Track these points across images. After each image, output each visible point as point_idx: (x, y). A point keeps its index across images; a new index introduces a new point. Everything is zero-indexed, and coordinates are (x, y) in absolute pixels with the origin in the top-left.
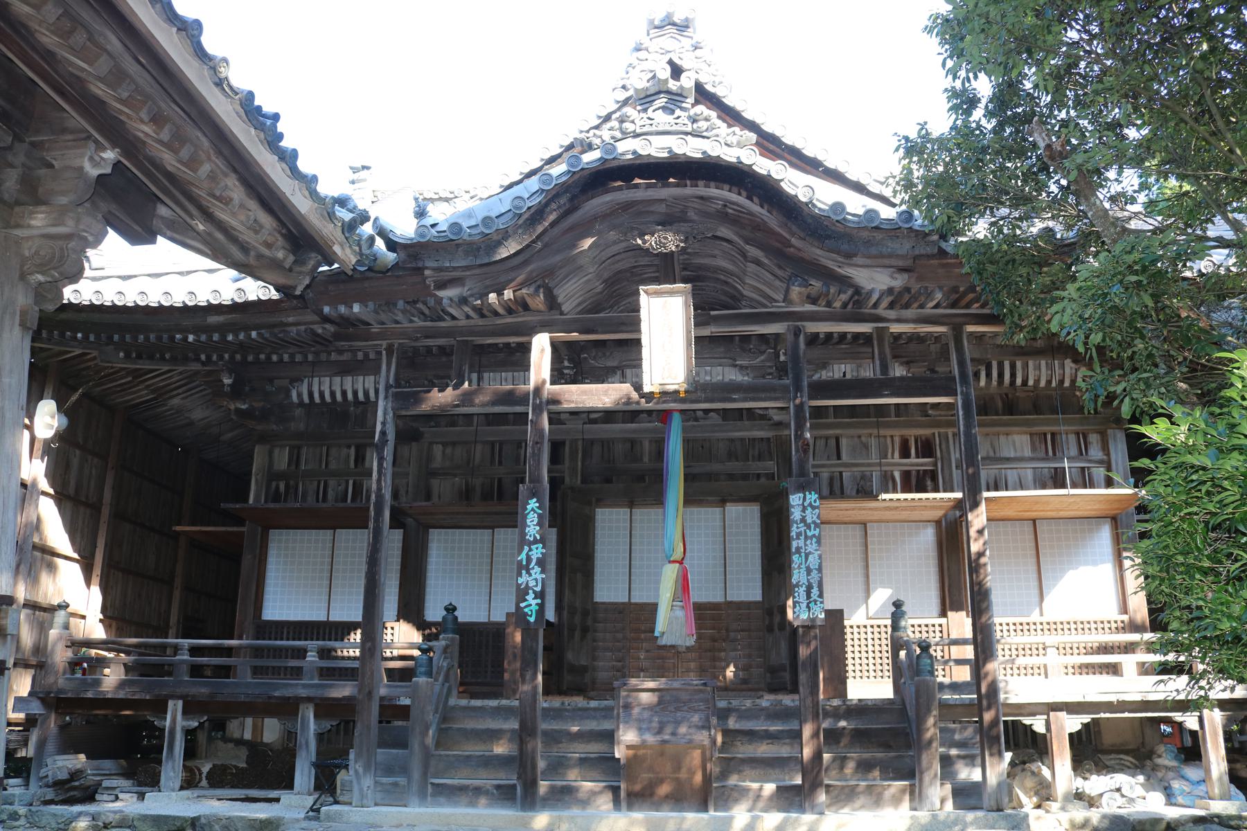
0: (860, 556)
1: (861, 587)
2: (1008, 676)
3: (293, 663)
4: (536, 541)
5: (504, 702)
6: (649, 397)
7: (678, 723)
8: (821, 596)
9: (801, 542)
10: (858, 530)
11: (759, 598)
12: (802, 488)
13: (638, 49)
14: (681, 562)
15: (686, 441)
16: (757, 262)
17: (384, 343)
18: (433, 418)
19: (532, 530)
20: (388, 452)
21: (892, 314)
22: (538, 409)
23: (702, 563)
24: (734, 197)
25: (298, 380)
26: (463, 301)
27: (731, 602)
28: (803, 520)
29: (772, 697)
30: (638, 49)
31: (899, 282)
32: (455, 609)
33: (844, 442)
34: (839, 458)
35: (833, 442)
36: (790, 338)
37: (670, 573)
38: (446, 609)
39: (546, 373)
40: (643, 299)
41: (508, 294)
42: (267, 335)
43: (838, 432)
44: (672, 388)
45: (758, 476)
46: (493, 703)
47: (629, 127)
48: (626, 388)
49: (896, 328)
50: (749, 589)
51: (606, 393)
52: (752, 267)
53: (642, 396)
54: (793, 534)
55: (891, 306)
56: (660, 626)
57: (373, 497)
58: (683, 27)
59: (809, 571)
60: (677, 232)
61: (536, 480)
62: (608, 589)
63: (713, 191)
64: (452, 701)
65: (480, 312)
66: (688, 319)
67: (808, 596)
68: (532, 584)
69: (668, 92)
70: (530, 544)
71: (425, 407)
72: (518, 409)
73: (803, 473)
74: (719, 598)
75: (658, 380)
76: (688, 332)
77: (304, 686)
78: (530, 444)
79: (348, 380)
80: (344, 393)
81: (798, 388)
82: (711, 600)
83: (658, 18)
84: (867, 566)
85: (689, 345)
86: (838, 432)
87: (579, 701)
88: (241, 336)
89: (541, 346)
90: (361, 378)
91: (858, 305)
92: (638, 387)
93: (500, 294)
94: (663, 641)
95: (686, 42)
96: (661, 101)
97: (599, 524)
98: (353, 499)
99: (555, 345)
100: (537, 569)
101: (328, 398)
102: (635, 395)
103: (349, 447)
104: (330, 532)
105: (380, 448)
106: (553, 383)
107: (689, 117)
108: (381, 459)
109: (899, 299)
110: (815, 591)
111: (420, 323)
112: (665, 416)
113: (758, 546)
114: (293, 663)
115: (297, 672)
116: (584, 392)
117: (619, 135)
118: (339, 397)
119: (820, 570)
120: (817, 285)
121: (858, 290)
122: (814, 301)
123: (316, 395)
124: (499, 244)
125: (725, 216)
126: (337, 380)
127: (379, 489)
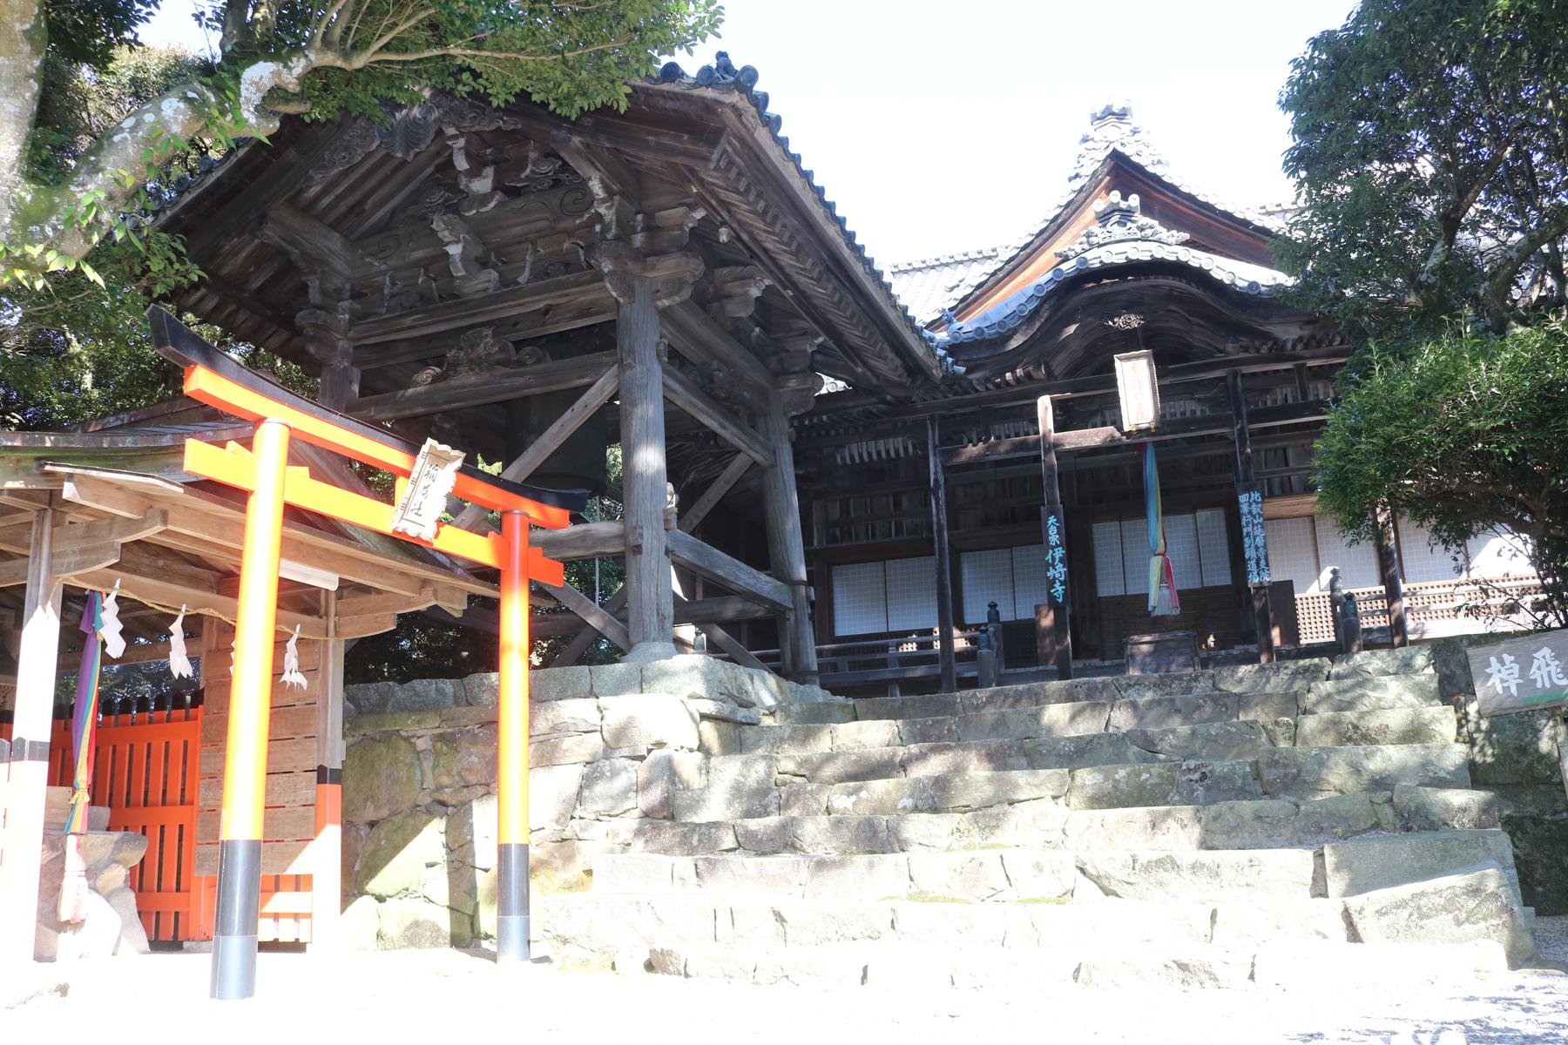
0: (1310, 542)
1: (1313, 566)
2: (1423, 620)
3: (880, 656)
4: (1057, 546)
5: (1041, 668)
6: (1129, 434)
7: (1169, 664)
8: (1267, 565)
9: (1250, 529)
10: (1307, 521)
11: (1229, 583)
12: (1248, 490)
13: (1085, 140)
14: (1163, 555)
15: (1160, 465)
16: (1198, 324)
17: (927, 415)
18: (970, 465)
19: (1054, 538)
20: (941, 493)
21: (1307, 353)
22: (1047, 451)
23: (1181, 553)
24: (1176, 283)
25: (841, 447)
26: (987, 380)
27: (1207, 588)
28: (1250, 512)
29: (1241, 647)
30: (1085, 140)
31: (1306, 332)
32: (996, 605)
33: (1290, 453)
34: (1287, 465)
35: (1281, 453)
36: (1230, 380)
37: (1156, 564)
38: (990, 606)
39: (1051, 425)
40: (1117, 364)
41: (1019, 372)
42: (835, 418)
43: (1284, 443)
44: (1144, 426)
45: (1221, 486)
46: (1034, 669)
47: (1094, 240)
48: (1110, 429)
49: (1310, 363)
50: (1223, 578)
51: (1096, 435)
52: (1196, 328)
53: (1124, 434)
54: (1244, 523)
55: (1306, 347)
56: (1152, 602)
57: (935, 527)
58: (1122, 115)
59: (1257, 548)
60: (1136, 313)
61: (1052, 502)
62: (1108, 588)
63: (1161, 281)
64: (1003, 671)
65: (998, 386)
66: (1152, 375)
67: (1258, 566)
68: (1057, 576)
69: (1120, 210)
70: (1053, 548)
71: (963, 458)
72: (1034, 453)
73: (1247, 479)
74: (1198, 586)
75: (1134, 422)
76: (1153, 384)
77: (890, 672)
78: (1045, 477)
79: (881, 443)
80: (879, 453)
81: (1239, 416)
82: (1191, 587)
83: (1099, 111)
84: (1317, 550)
85: (1154, 393)
86: (1284, 443)
87: (1097, 662)
88: (815, 421)
89: (1044, 405)
90: (891, 440)
91: (1278, 352)
92: (1120, 429)
93: (1013, 371)
94: (1157, 613)
95: (1126, 129)
96: (1116, 217)
97: (1096, 537)
98: (896, 535)
99: (1053, 402)
100: (1061, 565)
101: (848, 461)
102: (1118, 434)
103: (887, 495)
104: (880, 564)
105: (935, 491)
106: (1056, 430)
107: (1138, 228)
108: (937, 500)
109: (1308, 343)
110: (1263, 562)
111: (952, 397)
112: (1141, 447)
113: (1225, 541)
114: (880, 656)
115: (884, 664)
116: (1080, 436)
117: (1086, 247)
118: (875, 456)
119: (1265, 547)
120: (1245, 341)
121: (1276, 341)
122: (1246, 349)
123: (857, 457)
124: (1010, 338)
125: (1171, 296)
126: (872, 443)
127: (939, 520)
